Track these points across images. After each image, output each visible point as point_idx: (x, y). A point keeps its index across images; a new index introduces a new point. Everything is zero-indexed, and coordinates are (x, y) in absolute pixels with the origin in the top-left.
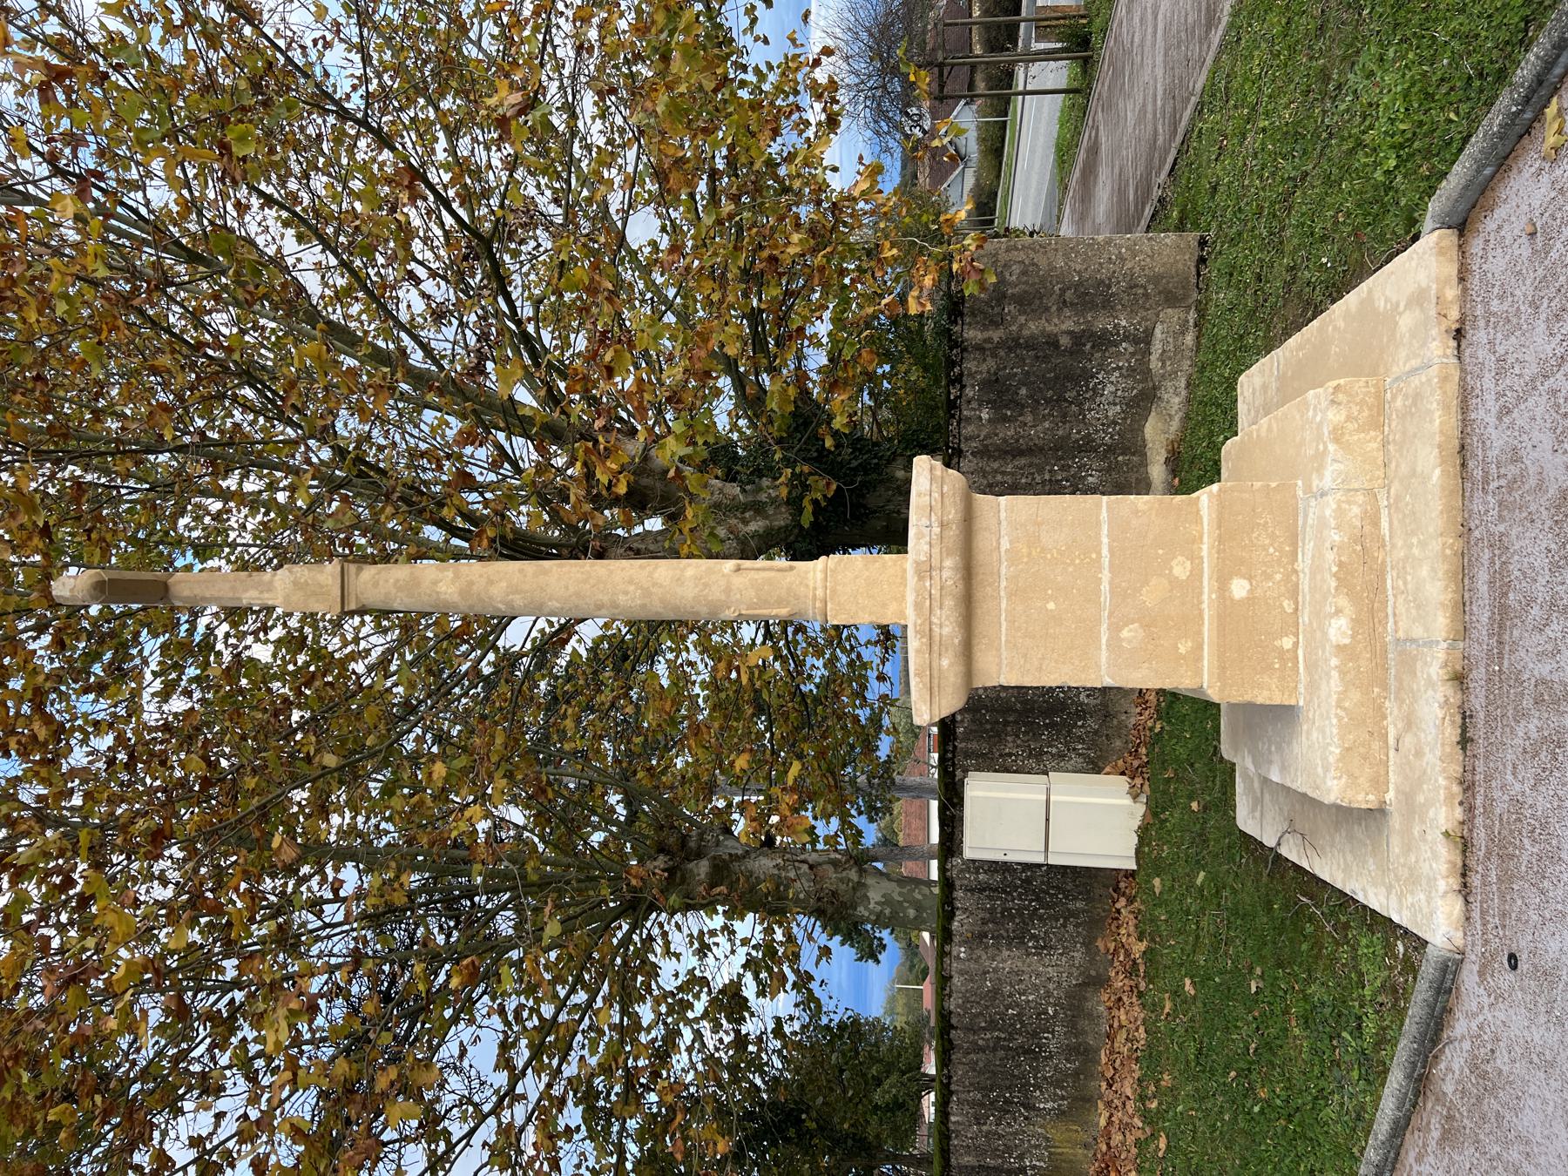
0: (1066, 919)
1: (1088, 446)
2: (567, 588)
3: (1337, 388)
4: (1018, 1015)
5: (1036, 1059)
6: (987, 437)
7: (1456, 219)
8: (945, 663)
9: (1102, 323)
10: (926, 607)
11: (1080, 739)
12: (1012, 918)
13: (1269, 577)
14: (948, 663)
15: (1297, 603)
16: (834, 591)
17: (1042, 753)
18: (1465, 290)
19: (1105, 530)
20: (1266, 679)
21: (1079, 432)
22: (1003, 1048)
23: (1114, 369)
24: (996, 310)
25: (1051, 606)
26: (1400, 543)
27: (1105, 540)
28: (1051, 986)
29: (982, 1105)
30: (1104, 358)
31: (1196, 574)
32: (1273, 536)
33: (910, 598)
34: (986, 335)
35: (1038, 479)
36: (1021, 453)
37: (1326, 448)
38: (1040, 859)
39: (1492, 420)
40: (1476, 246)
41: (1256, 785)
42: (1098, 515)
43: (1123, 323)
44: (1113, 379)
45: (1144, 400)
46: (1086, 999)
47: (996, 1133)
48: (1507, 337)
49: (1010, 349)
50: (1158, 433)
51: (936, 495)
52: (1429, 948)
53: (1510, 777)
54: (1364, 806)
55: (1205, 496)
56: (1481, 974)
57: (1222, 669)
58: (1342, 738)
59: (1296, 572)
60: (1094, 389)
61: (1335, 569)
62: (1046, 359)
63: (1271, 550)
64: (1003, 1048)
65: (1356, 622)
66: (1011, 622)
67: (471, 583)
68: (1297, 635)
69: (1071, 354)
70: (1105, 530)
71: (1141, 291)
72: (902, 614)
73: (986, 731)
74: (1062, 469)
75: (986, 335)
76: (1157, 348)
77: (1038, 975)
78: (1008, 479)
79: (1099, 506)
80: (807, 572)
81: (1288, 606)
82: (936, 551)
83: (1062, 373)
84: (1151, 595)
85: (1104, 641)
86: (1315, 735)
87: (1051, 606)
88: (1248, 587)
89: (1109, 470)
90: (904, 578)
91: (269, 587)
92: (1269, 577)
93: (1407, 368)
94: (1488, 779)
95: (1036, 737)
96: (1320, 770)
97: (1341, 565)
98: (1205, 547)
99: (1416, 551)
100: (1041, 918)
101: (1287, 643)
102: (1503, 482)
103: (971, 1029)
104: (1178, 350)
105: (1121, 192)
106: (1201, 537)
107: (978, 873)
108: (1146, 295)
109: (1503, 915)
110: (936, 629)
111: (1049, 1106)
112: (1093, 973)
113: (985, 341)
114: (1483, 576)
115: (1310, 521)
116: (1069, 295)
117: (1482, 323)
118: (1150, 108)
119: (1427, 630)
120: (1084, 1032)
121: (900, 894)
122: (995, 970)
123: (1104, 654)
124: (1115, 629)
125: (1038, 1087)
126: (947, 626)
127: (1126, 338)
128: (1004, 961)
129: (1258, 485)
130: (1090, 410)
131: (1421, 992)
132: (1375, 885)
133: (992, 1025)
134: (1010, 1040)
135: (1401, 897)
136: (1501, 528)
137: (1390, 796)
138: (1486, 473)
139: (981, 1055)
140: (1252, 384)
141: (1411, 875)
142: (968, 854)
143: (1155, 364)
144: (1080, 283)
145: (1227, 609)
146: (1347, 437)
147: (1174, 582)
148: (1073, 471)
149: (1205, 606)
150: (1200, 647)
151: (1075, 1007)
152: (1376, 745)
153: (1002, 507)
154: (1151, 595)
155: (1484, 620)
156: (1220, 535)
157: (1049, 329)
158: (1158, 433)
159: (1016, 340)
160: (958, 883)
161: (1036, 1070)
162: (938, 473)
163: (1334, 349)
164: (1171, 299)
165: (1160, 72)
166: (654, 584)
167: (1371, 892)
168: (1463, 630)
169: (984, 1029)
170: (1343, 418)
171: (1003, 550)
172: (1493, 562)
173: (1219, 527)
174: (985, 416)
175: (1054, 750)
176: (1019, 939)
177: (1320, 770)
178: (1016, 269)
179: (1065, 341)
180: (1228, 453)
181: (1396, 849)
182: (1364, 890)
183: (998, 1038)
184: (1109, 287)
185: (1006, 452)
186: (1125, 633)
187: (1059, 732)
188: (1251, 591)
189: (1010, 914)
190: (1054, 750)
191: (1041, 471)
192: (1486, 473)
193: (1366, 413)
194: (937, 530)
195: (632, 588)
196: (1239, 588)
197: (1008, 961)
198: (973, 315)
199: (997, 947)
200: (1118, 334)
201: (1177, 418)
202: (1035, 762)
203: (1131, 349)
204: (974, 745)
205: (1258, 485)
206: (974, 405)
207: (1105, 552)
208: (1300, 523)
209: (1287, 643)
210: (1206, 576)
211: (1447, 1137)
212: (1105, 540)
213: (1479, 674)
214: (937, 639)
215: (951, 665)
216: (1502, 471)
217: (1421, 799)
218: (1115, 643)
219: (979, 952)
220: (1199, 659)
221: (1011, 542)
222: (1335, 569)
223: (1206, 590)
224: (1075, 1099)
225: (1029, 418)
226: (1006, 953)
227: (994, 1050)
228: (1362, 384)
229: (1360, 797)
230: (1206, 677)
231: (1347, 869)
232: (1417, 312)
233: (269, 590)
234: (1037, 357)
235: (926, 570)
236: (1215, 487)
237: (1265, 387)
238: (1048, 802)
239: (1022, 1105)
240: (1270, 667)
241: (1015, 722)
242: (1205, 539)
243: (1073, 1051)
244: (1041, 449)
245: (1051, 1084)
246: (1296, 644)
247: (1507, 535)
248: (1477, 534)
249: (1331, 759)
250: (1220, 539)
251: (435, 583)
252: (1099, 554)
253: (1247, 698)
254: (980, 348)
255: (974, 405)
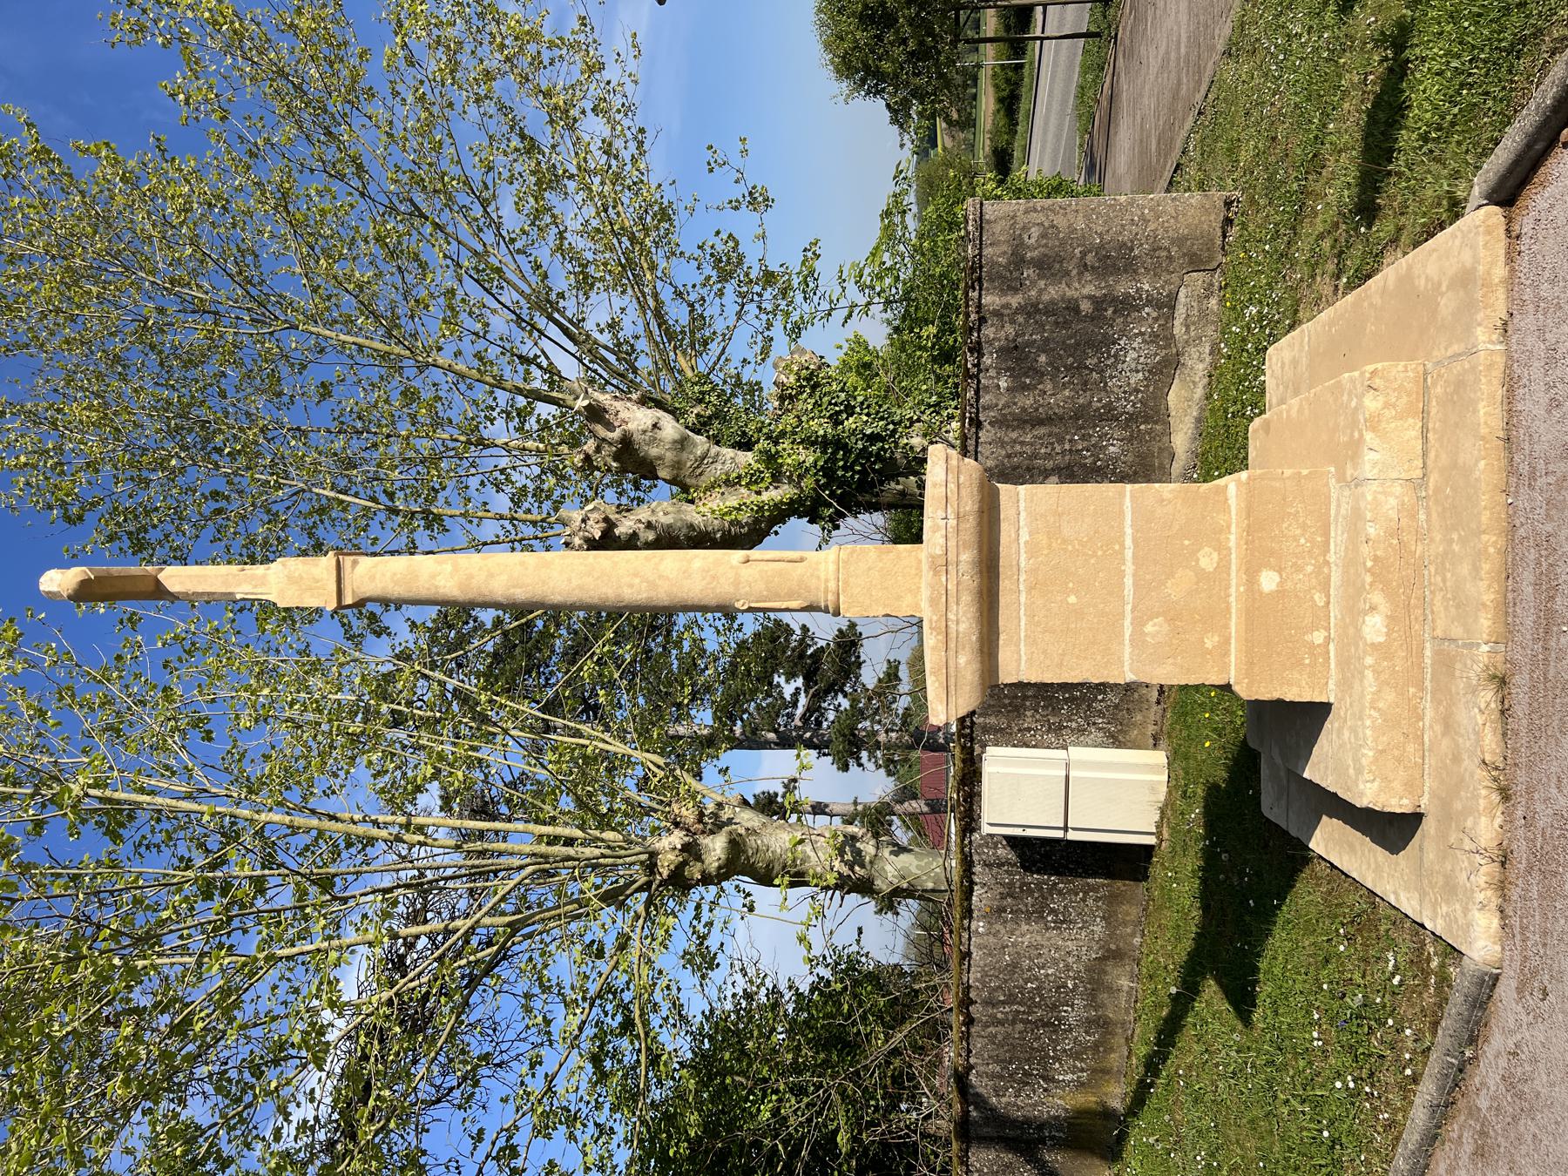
0: (1086, 893)
1: (1109, 415)
2: (569, 580)
3: (1374, 373)
4: (1037, 988)
5: (1055, 1032)
6: (1006, 406)
7: (1503, 196)
8: (962, 660)
9: (1124, 287)
10: (944, 600)
11: (1101, 714)
12: (1030, 892)
13: (1299, 569)
14: (966, 663)
15: (1328, 596)
16: (846, 583)
17: (1061, 728)
18: (1513, 270)
19: (1128, 521)
20: (1296, 675)
21: (1100, 400)
22: (1022, 1021)
23: (1136, 335)
24: (1016, 274)
25: (1072, 599)
26: (1438, 537)
27: (1129, 531)
28: (1070, 960)
29: (1001, 1077)
30: (1126, 324)
31: (1223, 566)
32: (1304, 527)
33: (925, 593)
34: (1004, 300)
35: (1058, 449)
36: (1041, 422)
37: (1361, 436)
38: (1059, 834)
39: (1540, 412)
40: (1526, 224)
41: (1282, 774)
42: (1121, 504)
43: (1146, 287)
44: (1135, 345)
45: (1166, 369)
46: (1105, 973)
47: (1015, 1104)
48: (1558, 325)
49: (1029, 315)
50: (1184, 402)
51: (952, 486)
52: (1465, 960)
53: (1554, 791)
54: (1398, 811)
55: (1231, 485)
56: (1520, 990)
57: (1249, 665)
58: (1376, 740)
59: (1327, 563)
60: (1116, 356)
61: (1369, 564)
62: (1066, 324)
63: (1302, 541)
64: (1022, 1021)
65: (1391, 619)
66: (1031, 616)
67: (471, 577)
68: (1328, 629)
69: (1093, 319)
70: (1128, 521)
71: (1164, 254)
72: (917, 606)
73: (1005, 706)
74: (1083, 438)
75: (1004, 300)
76: (1181, 311)
77: (1057, 949)
78: (1028, 449)
79: (1122, 495)
80: (818, 563)
81: (1319, 599)
82: (952, 543)
83: (1080, 338)
84: (1176, 588)
85: (1127, 636)
86: (1346, 733)
87: (1072, 599)
88: (1278, 579)
89: (1130, 440)
90: (919, 568)
91: (263, 580)
92: (1299, 569)
93: (1449, 353)
94: (1530, 791)
95: (1056, 711)
96: (1351, 771)
97: (1376, 559)
98: (1233, 537)
99: (1456, 548)
100: (1060, 893)
101: (1318, 637)
102: (1551, 479)
103: (990, 1003)
104: (1203, 314)
105: (1143, 143)
106: (1229, 527)
107: (996, 847)
108: (1170, 258)
109: (1545, 933)
110: (952, 626)
111: (1069, 1077)
112: (1113, 947)
113: (1003, 306)
114: (1528, 576)
115: (1343, 511)
116: (1090, 258)
117: (1531, 308)
118: (1173, 55)
119: (1467, 631)
120: (1103, 1006)
121: (918, 867)
122: (1014, 945)
123: (1127, 650)
124: (1139, 623)
125: (1057, 1059)
126: (965, 621)
127: (1149, 302)
128: (1023, 935)
129: (1288, 472)
130: (1111, 377)
131: (1457, 1003)
132: (1407, 889)
133: (1011, 999)
134: (1029, 1014)
135: (1435, 905)
136: (1549, 528)
137: (1424, 802)
138: (1533, 470)
139: (1000, 1028)
140: (1282, 358)
141: (1447, 883)
142: (986, 829)
143: (1178, 329)
144: (1102, 246)
145: (1255, 603)
146: (1383, 425)
147: (1201, 575)
148: (1093, 440)
149: (1232, 599)
150: (1227, 641)
151: (1095, 983)
152: (1411, 748)
153: (1022, 496)
154: (1176, 588)
155: (1529, 622)
156: (1249, 526)
157: (1069, 293)
158: (1184, 402)
159: (1035, 305)
160: (976, 858)
161: (1056, 1042)
162: (954, 462)
163: (1370, 328)
164: (1196, 263)
165: (1184, 18)
166: (660, 577)
167: (1403, 896)
168: (1507, 632)
169: (1003, 1002)
170: (1379, 405)
171: (1022, 541)
172: (1539, 564)
173: (1248, 517)
174: (1003, 384)
175: (1074, 725)
176: (1038, 913)
177: (1351, 771)
178: (1035, 232)
179: (1086, 306)
180: (1255, 431)
181: (1430, 855)
182: (1395, 893)
183: (1018, 1012)
184: (1132, 250)
185: (1025, 422)
186: (1149, 628)
187: (1078, 706)
188: (1281, 584)
189: (1029, 889)
190: (1074, 725)
191: (1061, 441)
192: (1533, 470)
193: (1405, 399)
194: (952, 522)
195: (637, 581)
196: (1269, 581)
197: (1027, 935)
198: (991, 280)
199: (1016, 922)
200: (1140, 298)
201: (1200, 386)
202: (1057, 734)
203: (1155, 314)
204: (992, 720)
205: (1288, 472)
206: (992, 373)
207: (1128, 542)
208: (1333, 512)
209: (1318, 637)
210: (1234, 568)
211: (1480, 1153)
212: (1129, 531)
213: (1520, 681)
214: (953, 635)
215: (968, 663)
216: (1551, 468)
217: (1458, 806)
218: (1138, 640)
219: (998, 927)
220: (1227, 653)
221: (1030, 534)
222: (1369, 564)
223: (1234, 582)
224: (1094, 1071)
225: (1049, 386)
226: (1025, 927)
227: (1013, 1023)
228: (1400, 368)
229: (1394, 801)
230: (1233, 673)
231: (1378, 869)
232: (1462, 293)
233: (263, 584)
234: (1057, 323)
235: (943, 565)
236: (1244, 475)
237: (1295, 363)
238: (1067, 777)
239: (1042, 1077)
240: (1300, 663)
241: (1035, 696)
242: (1233, 529)
243: (1089, 1024)
244: (1061, 418)
245: (1071, 1056)
246: (1328, 639)
247: (1555, 535)
248: (1522, 532)
249: (1364, 762)
250: (1249, 530)
251: (433, 576)
252: (1123, 546)
253: (1275, 695)
254: (997, 314)
255: (992, 373)
